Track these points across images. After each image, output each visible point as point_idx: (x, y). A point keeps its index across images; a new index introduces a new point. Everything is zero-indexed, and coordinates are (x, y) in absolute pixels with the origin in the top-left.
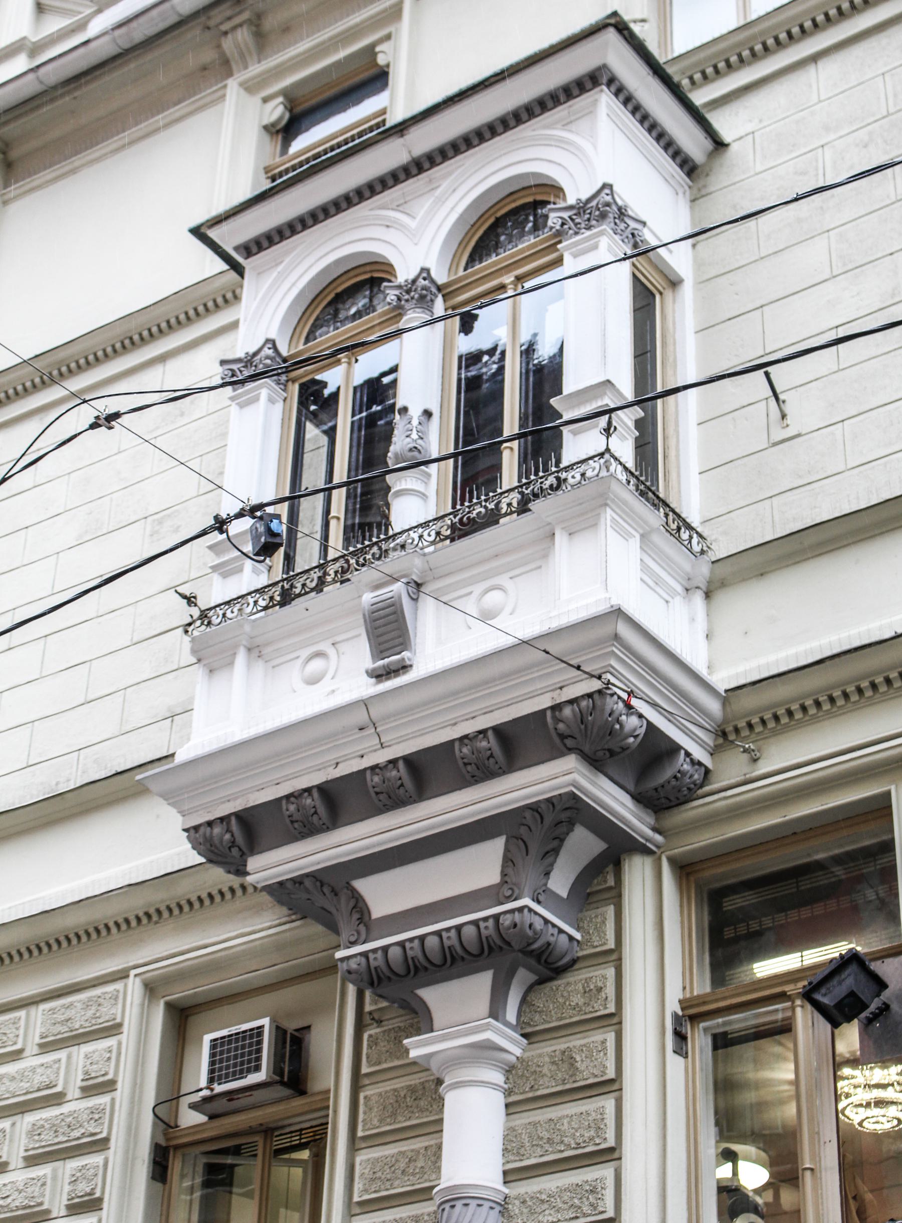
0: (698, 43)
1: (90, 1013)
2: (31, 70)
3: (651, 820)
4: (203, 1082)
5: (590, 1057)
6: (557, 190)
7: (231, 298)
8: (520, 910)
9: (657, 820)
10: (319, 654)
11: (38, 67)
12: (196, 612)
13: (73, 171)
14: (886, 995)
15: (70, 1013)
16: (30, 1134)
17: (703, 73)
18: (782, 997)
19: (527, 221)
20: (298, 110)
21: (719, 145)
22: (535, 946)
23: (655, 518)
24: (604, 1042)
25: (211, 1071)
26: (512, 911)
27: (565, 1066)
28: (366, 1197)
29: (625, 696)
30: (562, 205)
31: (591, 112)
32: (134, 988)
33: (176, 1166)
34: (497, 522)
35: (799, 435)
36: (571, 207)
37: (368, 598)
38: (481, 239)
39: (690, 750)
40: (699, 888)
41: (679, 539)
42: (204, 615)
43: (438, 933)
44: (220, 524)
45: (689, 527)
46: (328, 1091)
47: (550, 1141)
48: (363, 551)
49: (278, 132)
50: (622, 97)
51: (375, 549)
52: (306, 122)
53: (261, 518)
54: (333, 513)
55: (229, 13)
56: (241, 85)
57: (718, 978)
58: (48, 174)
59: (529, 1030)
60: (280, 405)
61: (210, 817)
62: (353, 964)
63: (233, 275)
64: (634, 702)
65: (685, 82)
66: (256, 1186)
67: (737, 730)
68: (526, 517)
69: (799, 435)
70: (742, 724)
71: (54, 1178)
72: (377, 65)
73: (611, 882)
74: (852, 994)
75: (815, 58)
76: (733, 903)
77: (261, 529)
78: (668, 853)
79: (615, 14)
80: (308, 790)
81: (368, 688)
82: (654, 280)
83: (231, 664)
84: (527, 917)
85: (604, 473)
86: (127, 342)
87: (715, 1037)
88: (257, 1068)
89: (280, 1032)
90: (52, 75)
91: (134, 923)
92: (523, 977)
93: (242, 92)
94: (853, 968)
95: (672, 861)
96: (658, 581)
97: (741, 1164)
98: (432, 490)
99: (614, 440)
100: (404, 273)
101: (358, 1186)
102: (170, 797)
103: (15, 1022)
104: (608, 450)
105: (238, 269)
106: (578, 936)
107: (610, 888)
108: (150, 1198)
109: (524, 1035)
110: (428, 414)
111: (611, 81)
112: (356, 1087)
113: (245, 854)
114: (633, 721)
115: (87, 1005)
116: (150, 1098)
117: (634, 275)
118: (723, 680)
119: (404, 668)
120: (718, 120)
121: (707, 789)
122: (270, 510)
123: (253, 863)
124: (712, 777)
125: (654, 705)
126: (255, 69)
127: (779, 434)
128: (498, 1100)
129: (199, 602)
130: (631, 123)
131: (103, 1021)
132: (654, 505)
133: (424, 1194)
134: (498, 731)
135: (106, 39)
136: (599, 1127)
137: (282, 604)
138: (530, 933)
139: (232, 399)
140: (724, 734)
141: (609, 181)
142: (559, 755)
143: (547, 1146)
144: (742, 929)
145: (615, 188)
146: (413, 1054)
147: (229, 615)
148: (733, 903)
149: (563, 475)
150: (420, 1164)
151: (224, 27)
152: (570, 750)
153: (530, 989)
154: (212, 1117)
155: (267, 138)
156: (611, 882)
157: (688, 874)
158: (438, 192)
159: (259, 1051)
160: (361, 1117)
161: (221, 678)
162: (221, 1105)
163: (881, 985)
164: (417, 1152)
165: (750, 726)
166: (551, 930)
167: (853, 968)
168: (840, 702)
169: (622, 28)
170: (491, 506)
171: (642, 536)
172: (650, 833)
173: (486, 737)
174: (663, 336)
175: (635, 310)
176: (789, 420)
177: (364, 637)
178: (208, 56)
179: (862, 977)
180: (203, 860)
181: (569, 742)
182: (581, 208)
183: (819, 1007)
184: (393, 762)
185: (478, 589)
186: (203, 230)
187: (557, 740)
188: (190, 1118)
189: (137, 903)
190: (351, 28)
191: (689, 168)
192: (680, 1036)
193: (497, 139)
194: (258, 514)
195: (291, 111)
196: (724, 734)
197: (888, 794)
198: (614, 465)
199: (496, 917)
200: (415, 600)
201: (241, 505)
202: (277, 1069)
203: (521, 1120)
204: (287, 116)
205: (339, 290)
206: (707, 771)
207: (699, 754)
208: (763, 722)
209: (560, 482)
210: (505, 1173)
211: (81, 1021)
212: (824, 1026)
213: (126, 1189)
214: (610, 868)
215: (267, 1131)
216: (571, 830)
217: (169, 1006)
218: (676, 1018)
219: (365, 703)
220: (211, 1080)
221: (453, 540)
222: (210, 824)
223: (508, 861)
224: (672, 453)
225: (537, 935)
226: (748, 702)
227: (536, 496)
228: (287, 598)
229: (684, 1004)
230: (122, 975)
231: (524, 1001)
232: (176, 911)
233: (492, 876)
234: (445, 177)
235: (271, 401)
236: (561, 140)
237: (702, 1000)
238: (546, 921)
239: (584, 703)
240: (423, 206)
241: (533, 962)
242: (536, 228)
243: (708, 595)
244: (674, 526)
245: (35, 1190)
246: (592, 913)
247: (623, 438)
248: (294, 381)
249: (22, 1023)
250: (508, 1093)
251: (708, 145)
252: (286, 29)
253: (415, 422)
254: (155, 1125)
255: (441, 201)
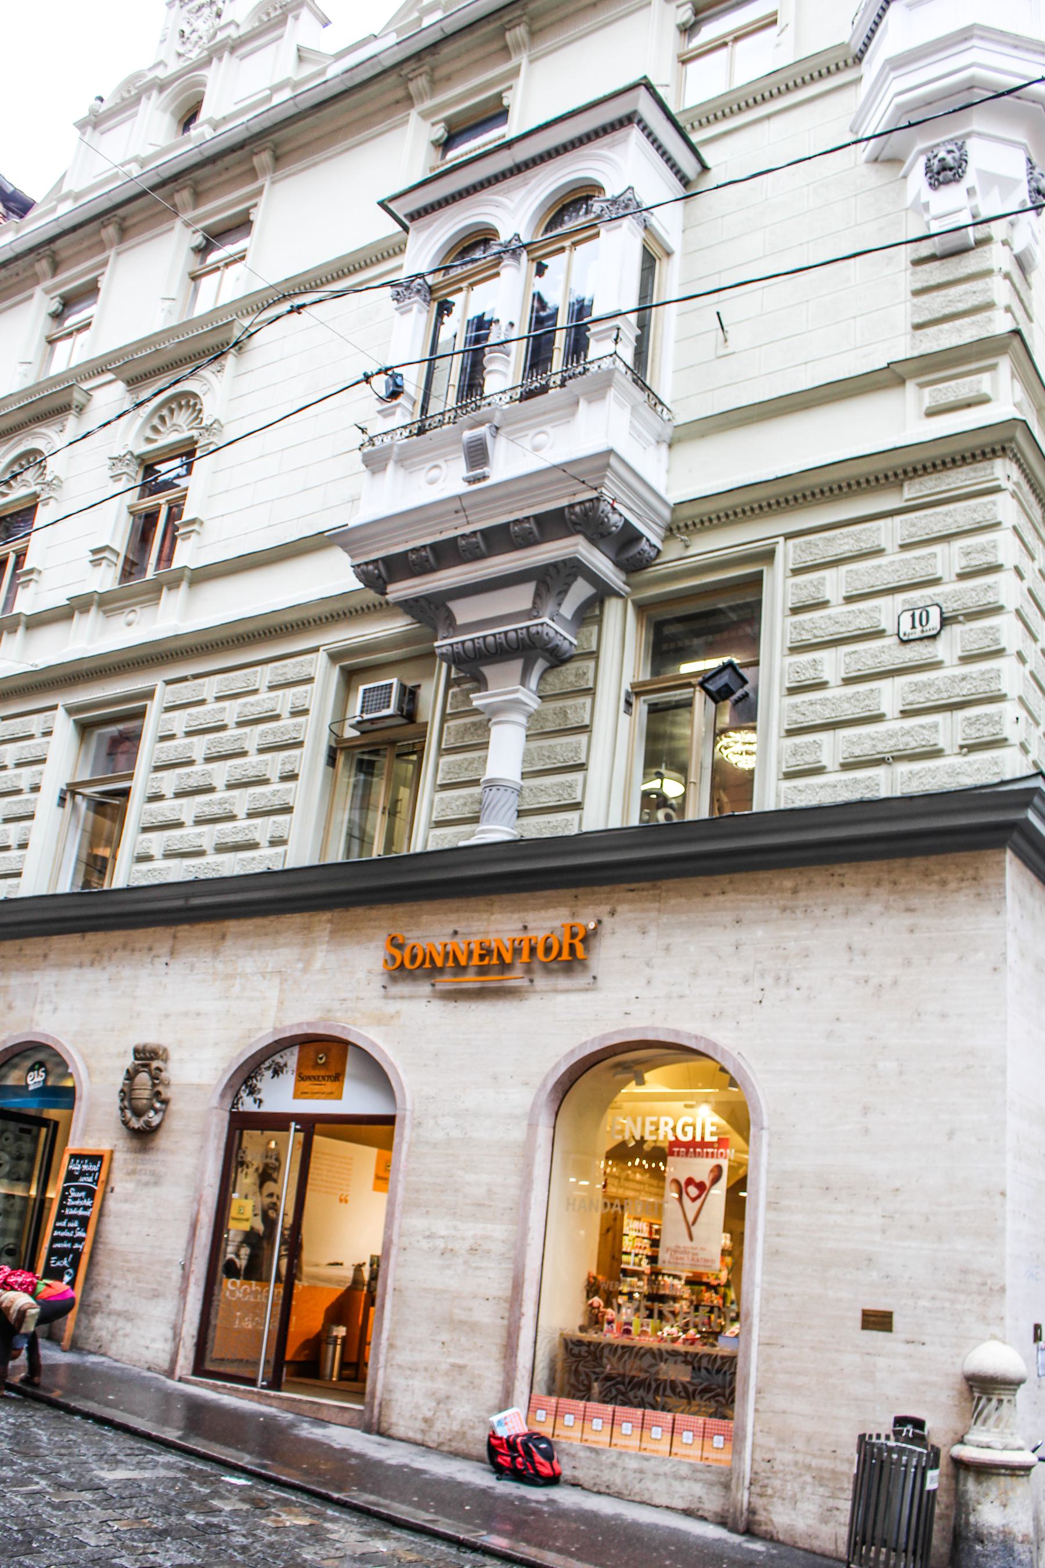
0: (698, 102)
1: (297, 670)
2: (291, 98)
3: (623, 577)
4: (358, 713)
5: (576, 711)
6: (600, 189)
7: (399, 249)
8: (542, 624)
9: (627, 577)
10: (436, 466)
11: (296, 96)
12: (366, 438)
13: (315, 165)
14: (747, 688)
15: (285, 670)
16: (261, 736)
17: (700, 122)
18: (689, 685)
19: (581, 208)
20: (453, 132)
21: (705, 168)
22: (550, 646)
23: (641, 396)
24: (584, 704)
25: (363, 707)
26: (537, 625)
27: (561, 716)
28: (445, 782)
29: (611, 501)
30: (602, 198)
31: (625, 140)
32: (322, 657)
33: (341, 759)
34: (547, 392)
35: (733, 353)
36: (608, 200)
37: (467, 434)
38: (553, 218)
39: (650, 538)
40: (649, 619)
41: (655, 411)
42: (371, 439)
43: (494, 635)
44: (367, 378)
45: (661, 403)
46: (426, 723)
47: (549, 757)
48: (466, 406)
49: (440, 145)
50: (656, 145)
51: (473, 405)
52: (458, 140)
53: (391, 376)
54: (451, 382)
55: (414, 66)
56: (419, 114)
57: (656, 671)
58: (299, 166)
59: (542, 694)
60: (425, 315)
61: (366, 559)
62: (444, 650)
63: (405, 233)
64: (616, 505)
65: (689, 127)
66: (385, 771)
67: (678, 528)
68: (564, 389)
69: (733, 353)
70: (682, 525)
71: (273, 761)
72: (502, 105)
73: (597, 612)
74: (726, 685)
75: (768, 117)
76: (669, 630)
77: (391, 382)
78: (633, 597)
79: (645, 77)
80: (424, 547)
81: (464, 488)
82: (655, 250)
83: (384, 469)
84: (546, 629)
85: (612, 367)
86: (340, 273)
87: (650, 705)
88: (388, 707)
89: (403, 687)
90: (305, 102)
91: (324, 620)
92: (540, 665)
93: (419, 118)
94: (729, 671)
95: (634, 602)
96: (640, 435)
97: (665, 780)
98: (510, 371)
99: (620, 345)
100: (505, 236)
101: (440, 775)
102: (344, 547)
103: (255, 673)
104: (615, 353)
105: (406, 229)
106: (575, 642)
107: (597, 616)
108: (325, 775)
109: (540, 697)
110: (512, 324)
111: (640, 121)
112: (443, 721)
113: (386, 583)
114: (614, 518)
115: (295, 666)
116: (328, 719)
117: (644, 247)
118: (673, 498)
119: (485, 477)
120: (705, 153)
121: (658, 561)
122: (397, 370)
123: (390, 588)
124: (662, 555)
125: (630, 509)
126: (428, 104)
127: (722, 351)
128: (522, 733)
129: (368, 432)
130: (651, 149)
131: (303, 676)
132: (642, 389)
133: (475, 782)
134: (536, 517)
135: (338, 80)
136: (577, 750)
137: (418, 435)
138: (546, 638)
139: (397, 309)
140: (671, 530)
141: (632, 185)
142: (570, 534)
143: (547, 761)
144: (672, 646)
145: (635, 190)
146: (475, 703)
147: (385, 440)
148: (669, 630)
149: (587, 366)
150: (475, 765)
151: (410, 76)
152: (578, 532)
153: (545, 671)
154: (362, 733)
155: (432, 148)
156: (597, 612)
157: (643, 611)
158: (529, 186)
159: (390, 697)
160: (444, 737)
161: (379, 477)
162: (367, 727)
163: (745, 682)
164: (474, 759)
165: (686, 526)
166: (559, 637)
167: (729, 671)
168: (740, 515)
169: (649, 87)
170: (543, 382)
171: (633, 408)
172: (622, 585)
173: (529, 522)
174: (659, 286)
175: (643, 270)
176: (728, 343)
177: (463, 459)
178: (400, 93)
179: (734, 675)
180: (362, 586)
181: (578, 528)
182: (614, 202)
183: (708, 692)
184: (474, 533)
185: (532, 433)
186: (386, 203)
187: (570, 525)
188: (350, 733)
189: (325, 610)
190: (487, 81)
191: (685, 182)
192: (629, 704)
193: (567, 154)
194: (390, 372)
195: (449, 132)
196: (671, 530)
197: (761, 573)
198: (618, 362)
199: (528, 628)
200: (494, 437)
201: (379, 367)
202: (400, 708)
203: (535, 744)
204: (446, 135)
205: (466, 245)
206: (659, 552)
207: (655, 541)
208: (694, 524)
209: (586, 370)
210: (522, 774)
211: (292, 675)
212: (711, 705)
213: (312, 770)
214: (598, 604)
215: (393, 743)
216: (575, 579)
217: (342, 668)
218: (628, 694)
219: (460, 497)
220: (362, 712)
221: (521, 401)
222: (367, 564)
223: (537, 595)
224: (657, 359)
225: (551, 640)
226: (687, 512)
227: (570, 378)
228: (421, 431)
229: (633, 686)
230: (316, 650)
231: (542, 678)
232: (348, 615)
233: (527, 604)
234: (534, 177)
235: (420, 312)
236: (605, 157)
237: (644, 684)
238: (557, 632)
239: (587, 505)
240: (519, 195)
241: (547, 655)
242: (587, 213)
243: (670, 446)
244: (653, 402)
245: (263, 767)
246: (585, 629)
247: (626, 346)
248: (434, 300)
249: (259, 674)
250: (528, 729)
251: (698, 168)
252: (448, 78)
253: (503, 329)
254: (330, 736)
255: (530, 192)
